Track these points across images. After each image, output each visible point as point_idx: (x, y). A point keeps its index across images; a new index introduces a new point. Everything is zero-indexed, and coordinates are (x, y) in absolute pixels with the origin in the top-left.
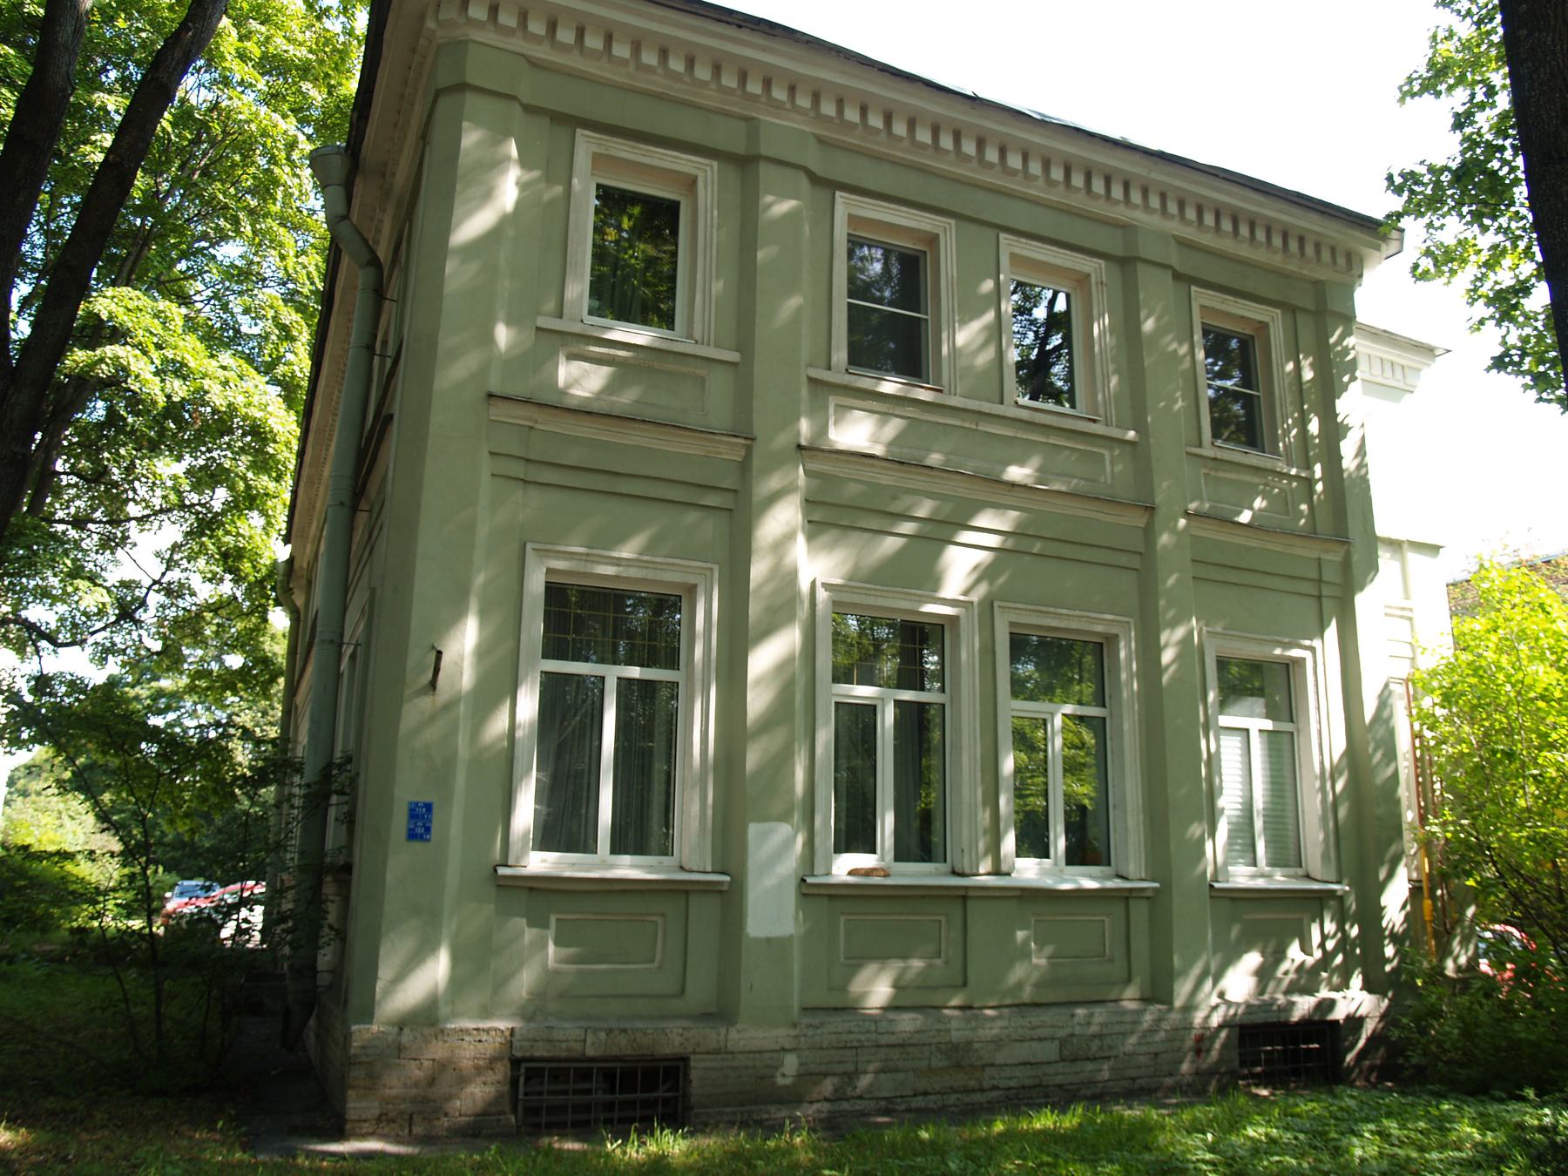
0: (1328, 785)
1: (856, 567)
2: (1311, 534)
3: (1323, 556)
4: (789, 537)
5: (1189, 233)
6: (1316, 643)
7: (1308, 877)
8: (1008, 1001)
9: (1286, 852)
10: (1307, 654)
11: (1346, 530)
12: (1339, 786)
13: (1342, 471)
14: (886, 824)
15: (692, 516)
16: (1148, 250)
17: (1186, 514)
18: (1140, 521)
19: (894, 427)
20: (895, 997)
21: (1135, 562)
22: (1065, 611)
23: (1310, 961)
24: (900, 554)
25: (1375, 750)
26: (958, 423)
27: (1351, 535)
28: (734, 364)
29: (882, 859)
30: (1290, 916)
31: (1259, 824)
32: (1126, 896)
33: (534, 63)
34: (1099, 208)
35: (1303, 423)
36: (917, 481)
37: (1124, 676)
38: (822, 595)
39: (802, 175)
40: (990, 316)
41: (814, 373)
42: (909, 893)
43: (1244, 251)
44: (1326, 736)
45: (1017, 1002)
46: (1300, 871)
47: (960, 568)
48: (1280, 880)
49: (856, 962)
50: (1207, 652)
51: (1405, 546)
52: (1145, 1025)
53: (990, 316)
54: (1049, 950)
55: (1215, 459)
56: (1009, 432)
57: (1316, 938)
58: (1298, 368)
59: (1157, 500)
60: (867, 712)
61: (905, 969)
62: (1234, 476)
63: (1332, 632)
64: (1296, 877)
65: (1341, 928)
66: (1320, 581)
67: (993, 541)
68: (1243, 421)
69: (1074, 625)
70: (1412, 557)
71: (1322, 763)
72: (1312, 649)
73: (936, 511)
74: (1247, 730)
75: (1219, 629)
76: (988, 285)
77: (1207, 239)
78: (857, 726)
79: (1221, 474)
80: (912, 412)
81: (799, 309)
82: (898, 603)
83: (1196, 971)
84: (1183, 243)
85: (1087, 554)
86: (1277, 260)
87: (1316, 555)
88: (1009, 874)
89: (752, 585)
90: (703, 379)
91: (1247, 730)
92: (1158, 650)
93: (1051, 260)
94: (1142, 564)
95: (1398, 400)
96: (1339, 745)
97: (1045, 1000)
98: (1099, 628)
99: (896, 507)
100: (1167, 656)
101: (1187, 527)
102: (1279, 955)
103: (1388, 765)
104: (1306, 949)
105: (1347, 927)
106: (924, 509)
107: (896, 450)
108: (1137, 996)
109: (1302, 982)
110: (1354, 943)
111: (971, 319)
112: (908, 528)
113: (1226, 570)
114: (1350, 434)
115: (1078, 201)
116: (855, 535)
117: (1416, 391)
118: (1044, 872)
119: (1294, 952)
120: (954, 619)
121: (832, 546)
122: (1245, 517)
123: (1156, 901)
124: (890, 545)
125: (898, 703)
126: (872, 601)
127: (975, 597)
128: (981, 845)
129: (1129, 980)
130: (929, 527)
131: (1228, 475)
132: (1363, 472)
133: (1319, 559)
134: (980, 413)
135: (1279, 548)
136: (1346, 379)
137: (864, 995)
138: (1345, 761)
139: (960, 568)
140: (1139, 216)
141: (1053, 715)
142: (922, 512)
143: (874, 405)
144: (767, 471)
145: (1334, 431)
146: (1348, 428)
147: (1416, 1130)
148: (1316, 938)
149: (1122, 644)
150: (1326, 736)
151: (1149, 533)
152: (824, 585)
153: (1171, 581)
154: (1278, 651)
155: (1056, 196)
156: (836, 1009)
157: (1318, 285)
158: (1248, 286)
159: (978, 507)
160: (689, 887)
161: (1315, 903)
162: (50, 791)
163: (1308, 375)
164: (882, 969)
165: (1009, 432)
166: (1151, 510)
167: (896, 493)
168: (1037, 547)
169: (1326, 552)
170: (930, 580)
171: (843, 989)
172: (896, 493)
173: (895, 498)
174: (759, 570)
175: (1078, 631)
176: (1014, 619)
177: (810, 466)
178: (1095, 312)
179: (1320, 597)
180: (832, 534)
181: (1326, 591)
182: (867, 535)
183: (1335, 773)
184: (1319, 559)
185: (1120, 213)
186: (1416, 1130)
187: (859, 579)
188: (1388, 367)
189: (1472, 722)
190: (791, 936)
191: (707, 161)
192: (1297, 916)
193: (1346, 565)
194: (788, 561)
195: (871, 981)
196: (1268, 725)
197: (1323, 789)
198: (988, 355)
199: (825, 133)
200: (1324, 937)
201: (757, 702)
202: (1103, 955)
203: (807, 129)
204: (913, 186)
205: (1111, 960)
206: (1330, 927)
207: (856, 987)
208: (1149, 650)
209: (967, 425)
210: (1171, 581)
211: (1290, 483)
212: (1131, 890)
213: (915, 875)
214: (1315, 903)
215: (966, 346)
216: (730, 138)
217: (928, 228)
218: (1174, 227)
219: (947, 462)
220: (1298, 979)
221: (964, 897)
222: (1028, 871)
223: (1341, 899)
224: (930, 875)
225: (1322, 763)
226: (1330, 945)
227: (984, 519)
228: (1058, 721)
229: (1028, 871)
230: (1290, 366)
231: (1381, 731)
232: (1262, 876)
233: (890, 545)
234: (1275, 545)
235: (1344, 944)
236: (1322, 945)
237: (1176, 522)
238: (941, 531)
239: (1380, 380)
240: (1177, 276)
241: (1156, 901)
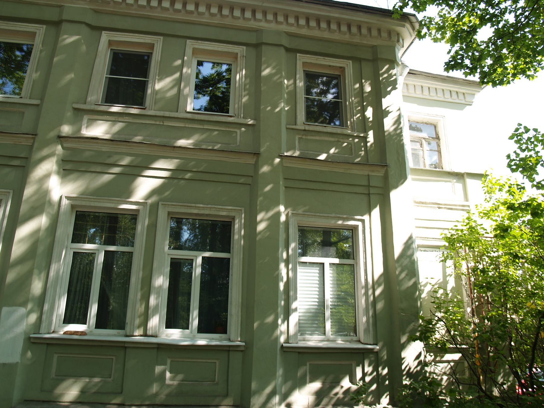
0: (370, 292)
1: (87, 188)
2: (363, 164)
3: (370, 174)
4: (47, 176)
5: (293, 30)
6: (366, 217)
7: (359, 341)
8: (147, 403)
9: (345, 327)
10: (360, 224)
11: (386, 160)
12: (378, 292)
13: (384, 132)
14: (93, 309)
15: (7, 170)
16: (266, 39)
17: (281, 156)
18: (251, 160)
19: (118, 127)
20: (79, 397)
21: (249, 180)
22: (201, 205)
23: (354, 387)
25: (401, 272)
26: (154, 122)
27: (388, 162)
28: (37, 105)
29: (89, 327)
30: (343, 363)
31: (328, 313)
32: (227, 350)
34: (241, 23)
35: (364, 110)
36: (123, 148)
37: (236, 237)
38: (65, 202)
39: (83, 26)
40: (177, 75)
41: (76, 106)
42: (118, 345)
43: (326, 35)
44: (372, 264)
45: (153, 403)
46: (355, 338)
47: (145, 186)
48: (340, 342)
49: (62, 377)
50: (290, 223)
51: (465, 176)
53: (177, 75)
54: (180, 377)
55: (305, 130)
57: (359, 374)
58: (362, 87)
59: (262, 150)
60: (91, 255)
61: (89, 382)
62: (317, 138)
63: (376, 212)
64: (350, 342)
65: (376, 369)
66: (369, 186)
68: (327, 113)
69: (207, 212)
70: (470, 182)
71: (366, 280)
72: (363, 221)
73: (132, 161)
74: (323, 264)
75: (300, 212)
76: (179, 62)
77: (304, 32)
78: (81, 265)
79: (309, 137)
80: (127, 119)
81: (71, 80)
82: (105, 205)
83: (268, 390)
84: (291, 35)
86: (347, 37)
87: (366, 173)
88: (155, 336)
89: (24, 198)
90: (24, 113)
91: (323, 264)
92: (255, 224)
93: (216, 49)
94: (251, 181)
95: (462, 109)
96: (379, 270)
97: (170, 403)
99: (110, 161)
100: (261, 227)
101: (280, 162)
102: (337, 382)
103: (410, 279)
104: (352, 381)
105: (380, 369)
106: (126, 161)
107: (116, 136)
108: (231, 403)
109: (346, 399)
110: (384, 378)
111: (167, 76)
112: (116, 170)
113: (301, 182)
114: (389, 115)
115: (228, 21)
116: (88, 175)
117: (473, 104)
118: (185, 337)
119: (346, 383)
120: (137, 211)
121: (75, 180)
122: (323, 157)
123: (245, 351)
124: (106, 178)
125: (106, 252)
126: (92, 204)
127: (150, 201)
128: (137, 322)
129: (226, 396)
130: (128, 170)
131: (314, 138)
132: (398, 131)
133: (368, 175)
134: (164, 117)
135: (341, 171)
136: (389, 89)
137: (61, 395)
138: (382, 279)
139: (145, 186)
140: (263, 24)
141: (196, 257)
142: (124, 163)
143: (108, 117)
144: (41, 148)
145: (381, 114)
146: (388, 113)
148: (359, 374)
149: (237, 221)
150: (372, 264)
151: (256, 167)
152: (66, 197)
153: (268, 188)
154: (340, 222)
155: (216, 20)
156: (44, 402)
157: (374, 48)
158: (331, 51)
160: (126, 345)
161: (358, 356)
163: (368, 89)
164: (75, 382)
166: (257, 154)
167: (110, 155)
169: (373, 171)
170: (127, 192)
171: (51, 391)
172: (110, 155)
173: (109, 157)
174: (28, 191)
175: (207, 215)
176: (171, 209)
177: (65, 145)
178: (238, 69)
179: (369, 194)
181: (372, 191)
182: (94, 174)
183: (375, 285)
184: (368, 175)
185: (252, 24)
187: (84, 195)
188: (454, 95)
189: (504, 262)
190: (17, 363)
191: (41, 26)
192: (347, 363)
193: (386, 177)
194: (45, 186)
195: (68, 388)
196: (336, 261)
197: (366, 294)
198: (174, 91)
199: (97, 8)
200: (364, 375)
201: (17, 250)
202: (214, 381)
203: (88, 7)
204: (142, 25)
205: (217, 384)
206: (368, 369)
207: (58, 391)
208: (251, 223)
209: (158, 123)
210: (268, 188)
211: (353, 140)
212: (230, 346)
213: (109, 335)
214: (358, 356)
215: (159, 90)
216: (51, 15)
217: (149, 41)
218: (284, 28)
219: (144, 140)
220: (344, 398)
221: (123, 347)
222: (174, 335)
223: (377, 353)
224: (115, 335)
225: (366, 280)
226: (368, 379)
227: (159, 164)
228: (199, 260)
229: (174, 335)
230: (357, 86)
231: (406, 262)
232: (328, 340)
233: (106, 178)
234: (340, 169)
235: (378, 379)
236: (363, 379)
237: (273, 160)
238: (135, 171)
239: (450, 100)
240: (288, 50)
241: (245, 351)
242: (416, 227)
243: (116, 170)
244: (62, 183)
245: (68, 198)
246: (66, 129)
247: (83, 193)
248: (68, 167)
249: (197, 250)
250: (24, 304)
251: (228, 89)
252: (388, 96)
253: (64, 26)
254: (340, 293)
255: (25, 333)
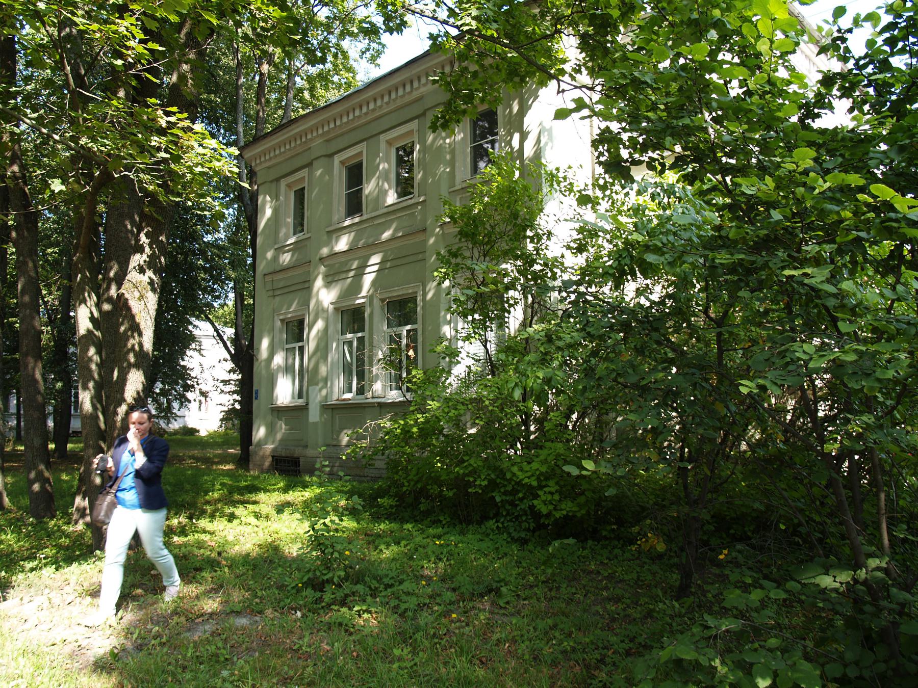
24: (352, 281)
33: (269, 168)
39: (322, 158)
52: (127, 44)
56: (383, 220)
67: (376, 268)
80: (355, 228)
85: (411, 259)
98: (410, 291)
112: (352, 274)
116: (340, 282)
143: (344, 231)
147: (665, 604)
159: (368, 258)
162: (228, 388)
165: (383, 220)
168: (388, 265)
175: (403, 295)
180: (334, 284)
186: (665, 604)
228: (405, 333)
242: (915, 207)
243: (352, 274)
244: (329, 292)
245: (332, 303)
246: (325, 251)
247: (339, 298)
248: (330, 279)
249: (400, 325)
250: (317, 384)
251: (237, 99)
252: (530, 111)
253: (315, 163)
254: (887, 35)
255: (320, 402)
